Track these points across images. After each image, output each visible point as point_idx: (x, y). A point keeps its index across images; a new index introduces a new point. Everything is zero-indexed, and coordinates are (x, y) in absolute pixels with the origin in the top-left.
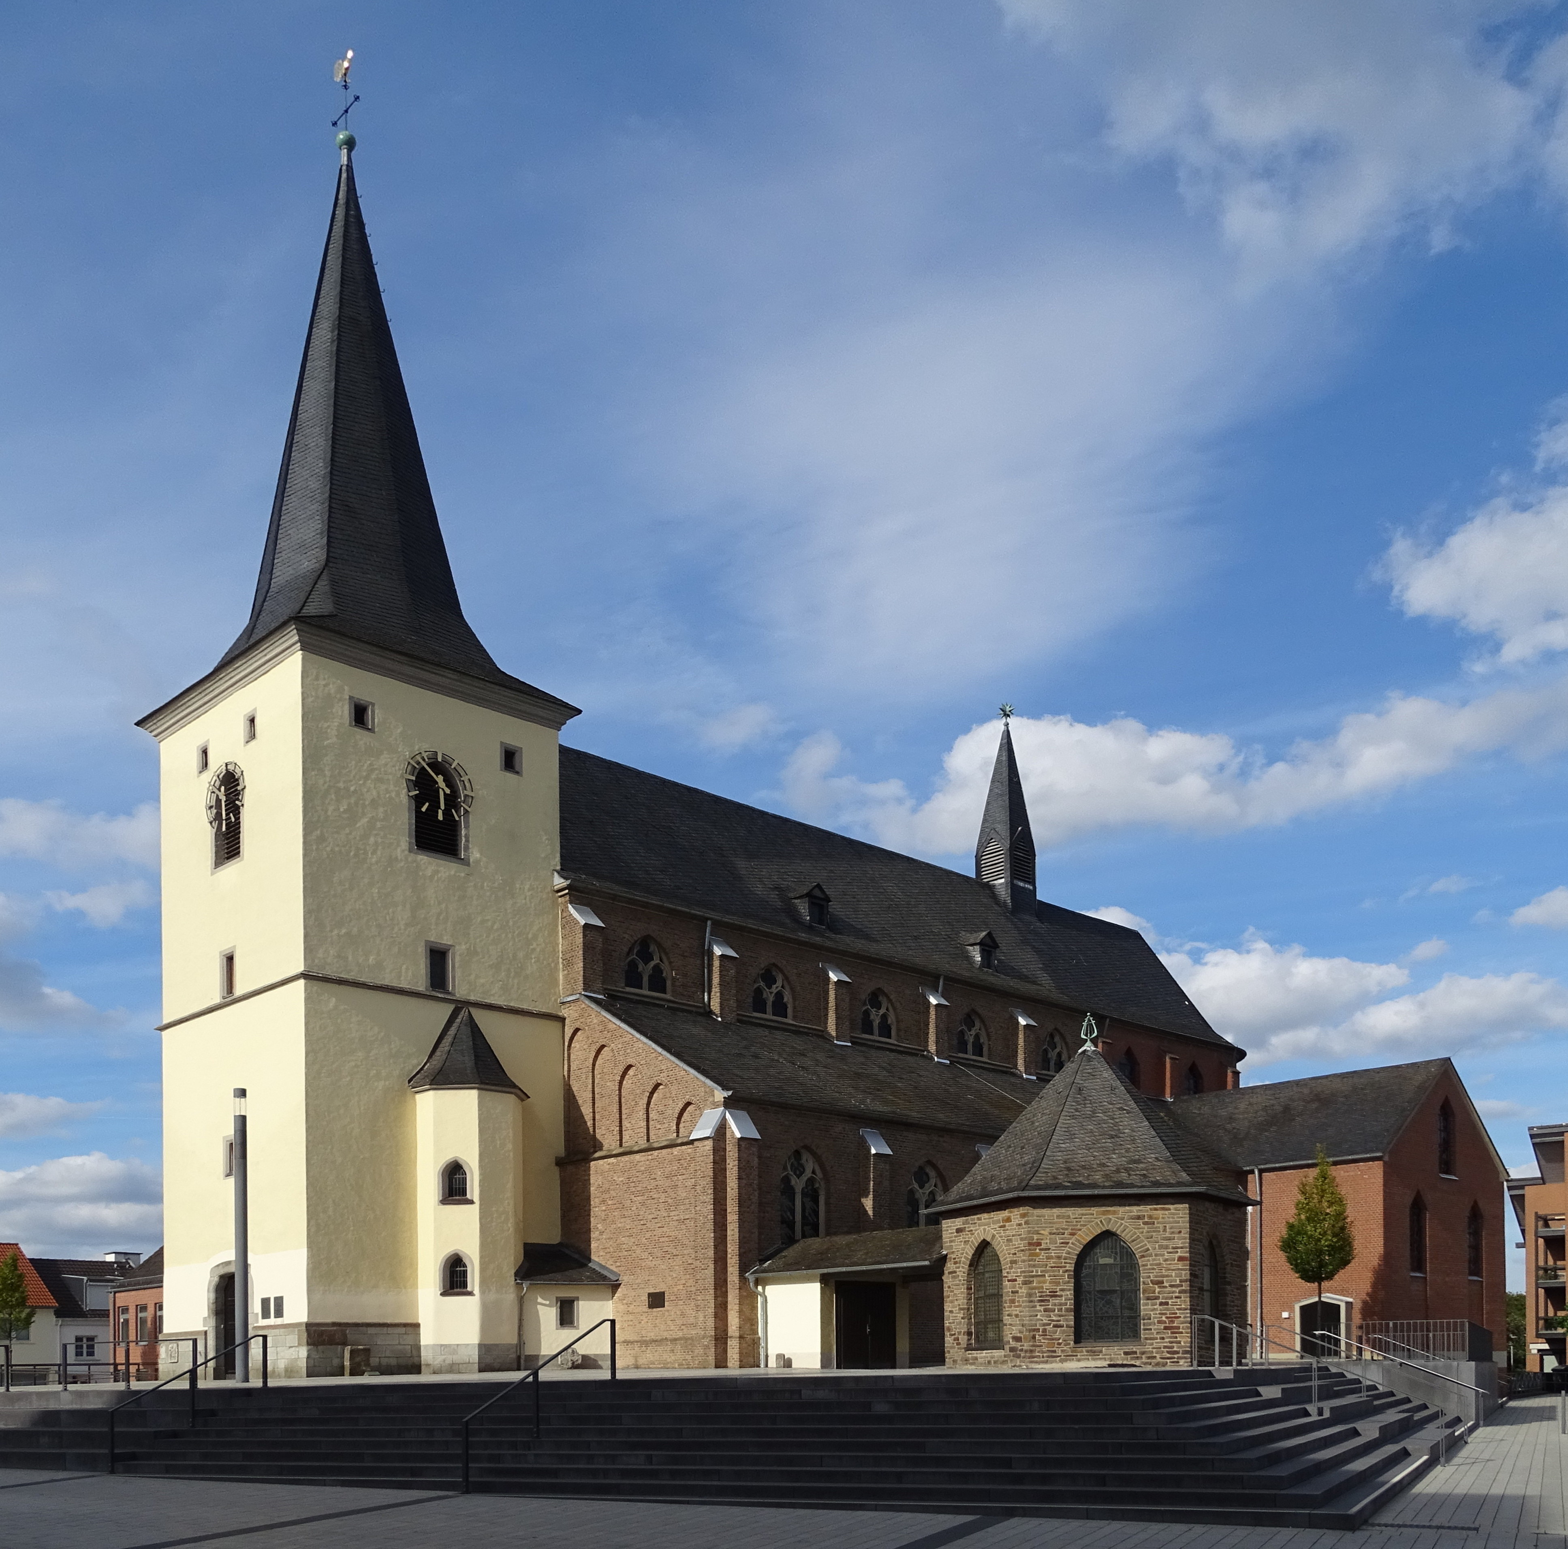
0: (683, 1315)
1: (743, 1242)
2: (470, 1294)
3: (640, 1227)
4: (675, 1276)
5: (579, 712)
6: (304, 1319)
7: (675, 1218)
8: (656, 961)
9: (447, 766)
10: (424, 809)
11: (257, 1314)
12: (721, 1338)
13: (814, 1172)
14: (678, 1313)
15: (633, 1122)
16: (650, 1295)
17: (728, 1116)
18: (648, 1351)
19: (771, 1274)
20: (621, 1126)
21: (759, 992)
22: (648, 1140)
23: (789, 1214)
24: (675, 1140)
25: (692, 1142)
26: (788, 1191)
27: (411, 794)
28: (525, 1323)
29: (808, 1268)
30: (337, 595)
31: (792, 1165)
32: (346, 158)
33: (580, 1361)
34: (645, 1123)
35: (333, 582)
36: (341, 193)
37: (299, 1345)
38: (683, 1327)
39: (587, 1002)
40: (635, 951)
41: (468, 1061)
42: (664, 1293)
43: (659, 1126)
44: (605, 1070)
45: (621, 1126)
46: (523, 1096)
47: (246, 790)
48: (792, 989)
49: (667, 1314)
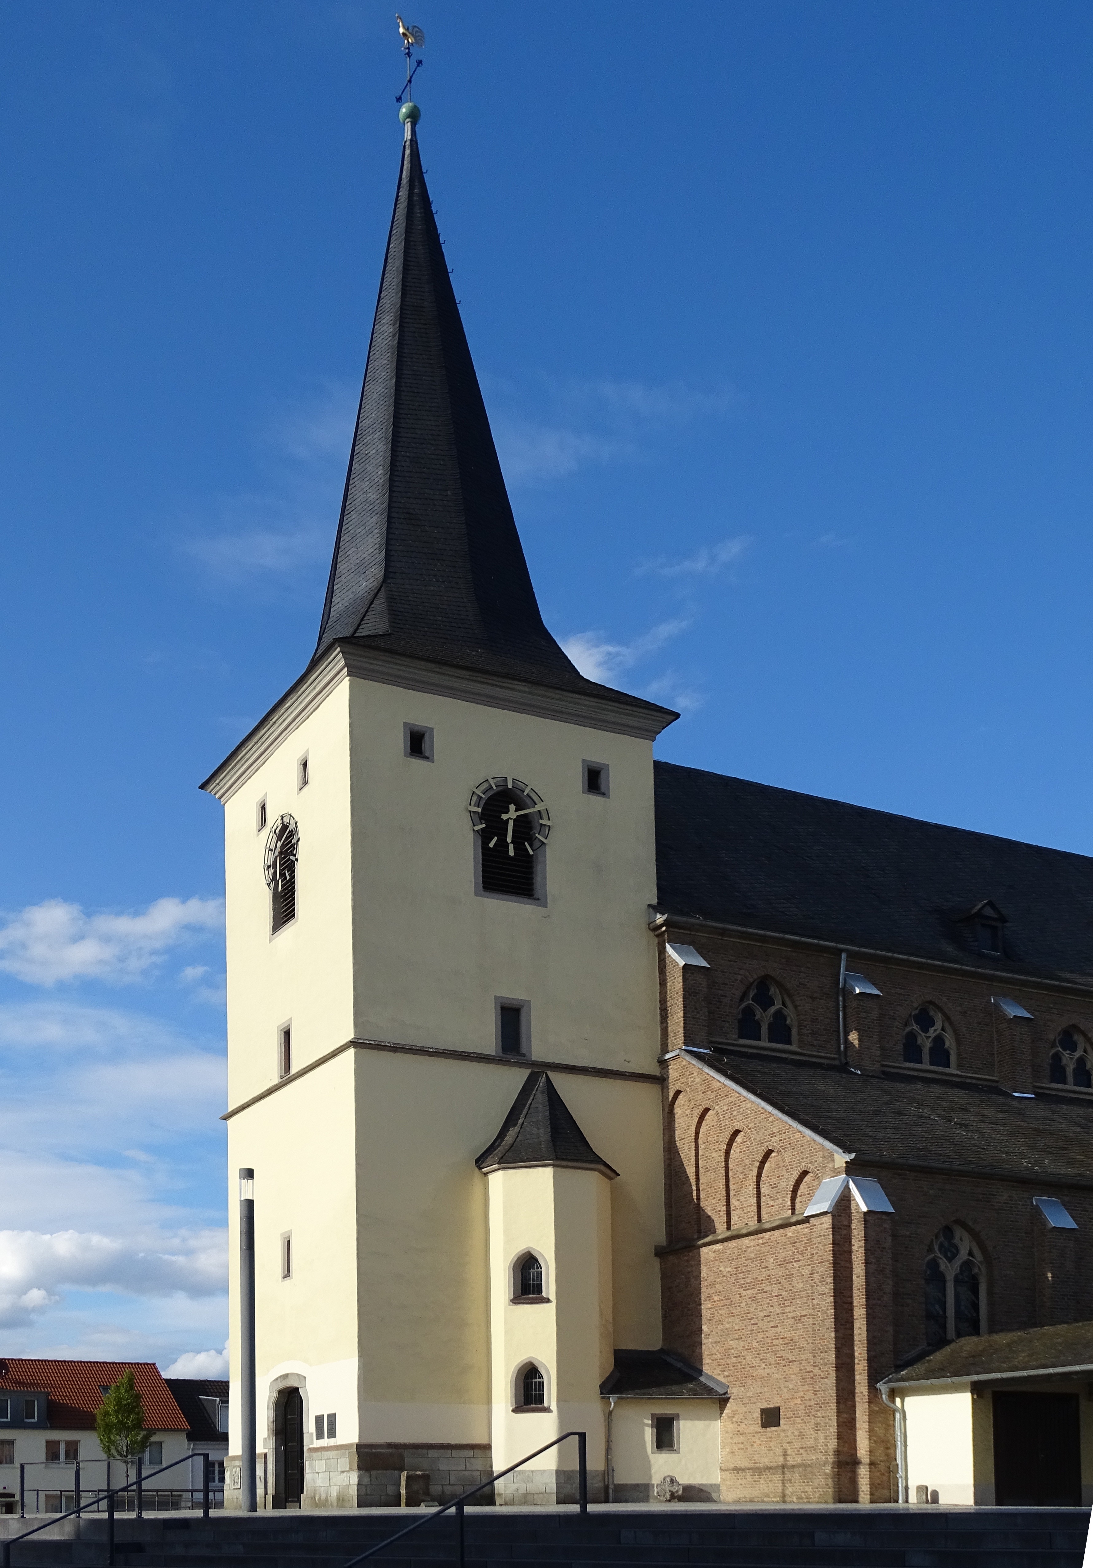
0: (802, 1435)
1: (872, 1342)
2: (547, 1410)
3: (750, 1328)
4: (791, 1386)
5: (677, 716)
6: (356, 1440)
7: (791, 1315)
8: (778, 1005)
9: (519, 792)
10: (491, 845)
11: (312, 1434)
12: (846, 1462)
13: (971, 1254)
14: (796, 1433)
15: (742, 1199)
16: (763, 1411)
17: (852, 1185)
18: (762, 1481)
19: (907, 1384)
20: (728, 1204)
21: (911, 1037)
22: (759, 1220)
23: (937, 1307)
24: (789, 1218)
25: (807, 1220)
26: (936, 1277)
27: (477, 828)
28: (613, 1446)
29: (955, 1374)
30: (394, 613)
31: (941, 1246)
32: (409, 133)
33: (680, 1493)
34: (755, 1200)
35: (390, 599)
36: (404, 172)
37: (351, 1469)
38: (802, 1451)
39: (688, 1058)
40: (751, 996)
41: (542, 1134)
42: (779, 1408)
43: (771, 1203)
44: (710, 1139)
45: (728, 1204)
46: (610, 1173)
47: (300, 843)
48: (956, 1033)
49: (783, 1434)
